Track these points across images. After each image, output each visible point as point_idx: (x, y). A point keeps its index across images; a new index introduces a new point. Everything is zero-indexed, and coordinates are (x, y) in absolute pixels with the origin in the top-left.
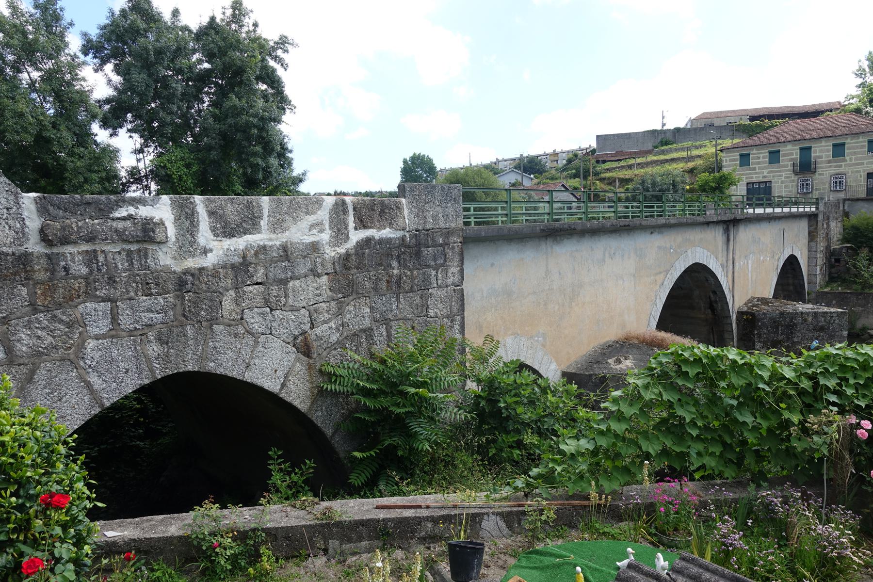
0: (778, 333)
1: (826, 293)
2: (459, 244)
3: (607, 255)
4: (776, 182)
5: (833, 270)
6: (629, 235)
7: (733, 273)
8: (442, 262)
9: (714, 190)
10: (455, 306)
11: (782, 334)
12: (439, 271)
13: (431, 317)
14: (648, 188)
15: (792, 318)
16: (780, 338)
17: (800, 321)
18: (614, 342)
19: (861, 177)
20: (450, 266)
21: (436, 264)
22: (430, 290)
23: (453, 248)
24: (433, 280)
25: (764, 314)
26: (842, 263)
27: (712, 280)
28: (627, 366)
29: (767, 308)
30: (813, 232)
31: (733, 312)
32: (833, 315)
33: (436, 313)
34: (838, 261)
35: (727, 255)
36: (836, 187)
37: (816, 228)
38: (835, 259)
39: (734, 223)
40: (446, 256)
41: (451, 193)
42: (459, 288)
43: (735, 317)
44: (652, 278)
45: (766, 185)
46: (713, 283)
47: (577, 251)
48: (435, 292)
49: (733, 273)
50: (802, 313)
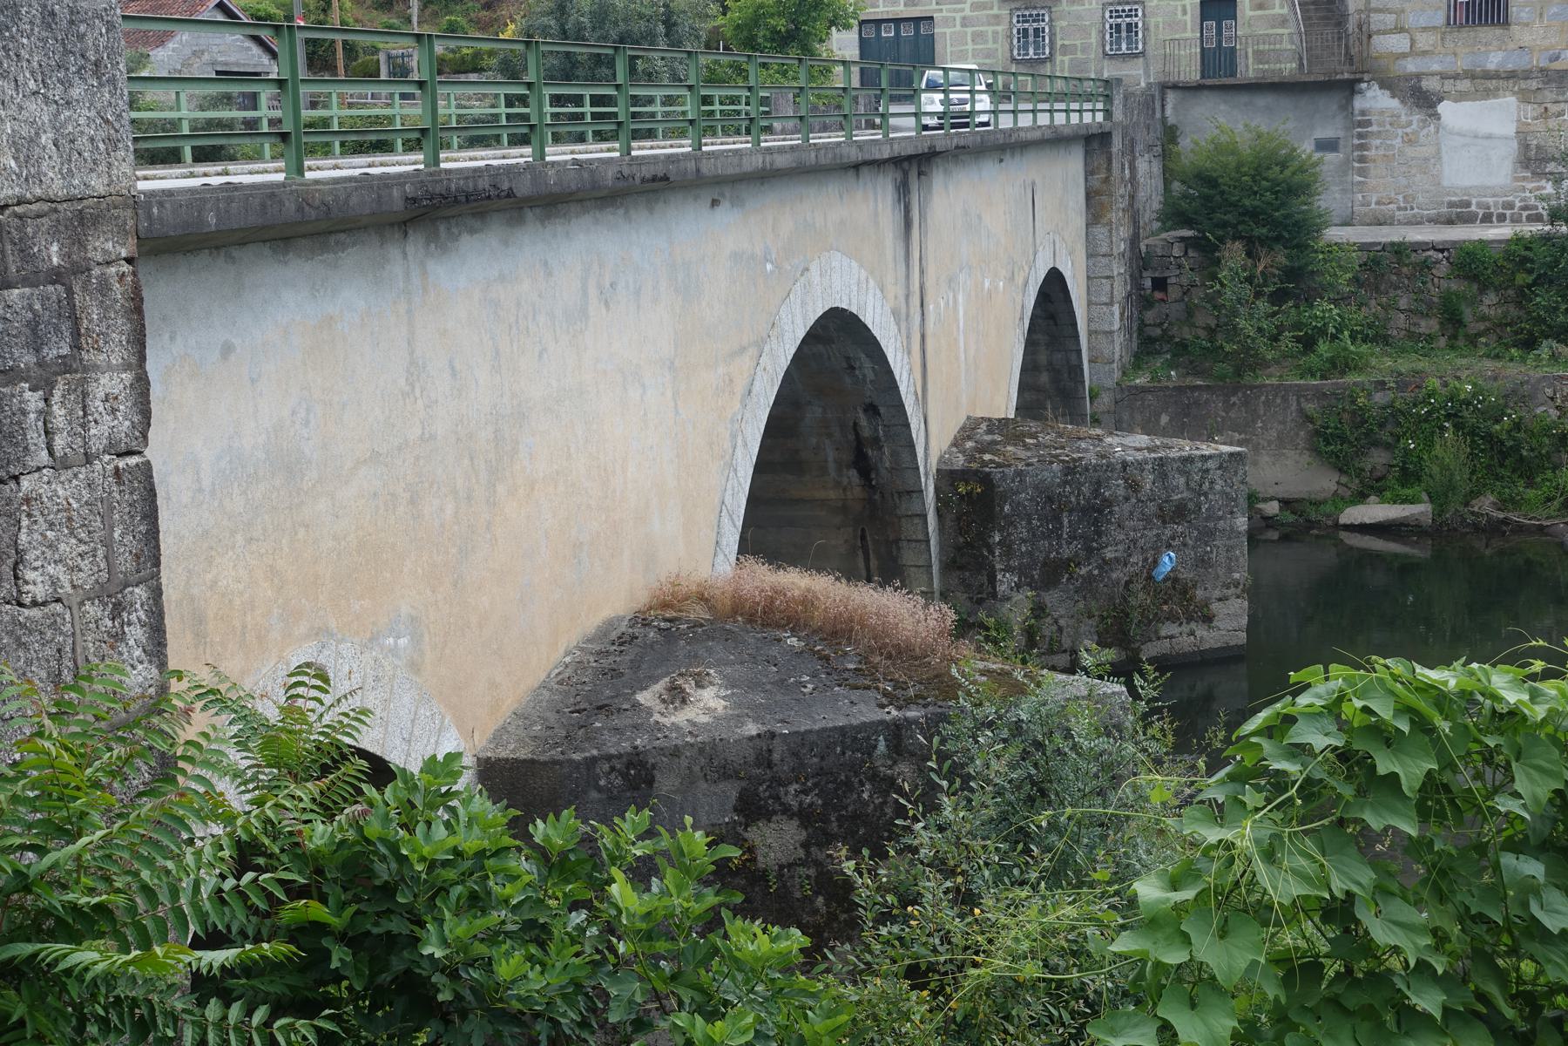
0: (1059, 537)
1: (1143, 390)
2: (126, 268)
3: (593, 292)
4: (948, 22)
5: (1150, 316)
6: (651, 211)
7: (923, 337)
8: (65, 351)
9: (782, 41)
10: (125, 542)
11: (1073, 537)
12: (57, 395)
13: (35, 604)
14: (580, 28)
15: (1099, 483)
16: (1067, 552)
17: (1121, 492)
18: (633, 621)
19: (1184, 12)
20: (96, 368)
21: (41, 364)
22: (25, 483)
23: (104, 287)
24: (35, 438)
25: (1019, 473)
26: (1174, 292)
27: (867, 368)
28: (708, 710)
29: (1022, 454)
30: (1098, 193)
31: (926, 474)
32: (1211, 464)
33: (55, 582)
34: (1160, 284)
35: (908, 277)
36: (1119, 43)
37: (1106, 180)
38: (1153, 279)
39: (879, 166)
40: (76, 321)
41: (81, 37)
42: (133, 460)
43: (931, 489)
44: (721, 370)
45: (917, 30)
46: (870, 375)
47: (502, 278)
48: (44, 490)
49: (923, 337)
50: (1125, 465)
